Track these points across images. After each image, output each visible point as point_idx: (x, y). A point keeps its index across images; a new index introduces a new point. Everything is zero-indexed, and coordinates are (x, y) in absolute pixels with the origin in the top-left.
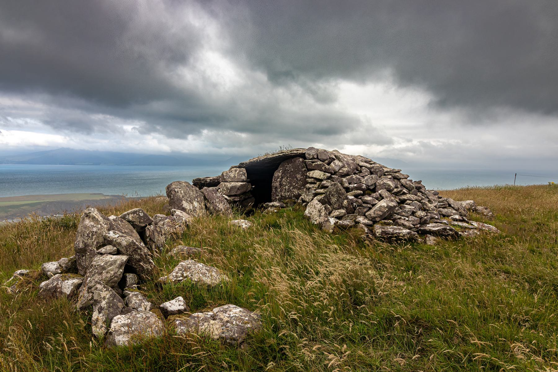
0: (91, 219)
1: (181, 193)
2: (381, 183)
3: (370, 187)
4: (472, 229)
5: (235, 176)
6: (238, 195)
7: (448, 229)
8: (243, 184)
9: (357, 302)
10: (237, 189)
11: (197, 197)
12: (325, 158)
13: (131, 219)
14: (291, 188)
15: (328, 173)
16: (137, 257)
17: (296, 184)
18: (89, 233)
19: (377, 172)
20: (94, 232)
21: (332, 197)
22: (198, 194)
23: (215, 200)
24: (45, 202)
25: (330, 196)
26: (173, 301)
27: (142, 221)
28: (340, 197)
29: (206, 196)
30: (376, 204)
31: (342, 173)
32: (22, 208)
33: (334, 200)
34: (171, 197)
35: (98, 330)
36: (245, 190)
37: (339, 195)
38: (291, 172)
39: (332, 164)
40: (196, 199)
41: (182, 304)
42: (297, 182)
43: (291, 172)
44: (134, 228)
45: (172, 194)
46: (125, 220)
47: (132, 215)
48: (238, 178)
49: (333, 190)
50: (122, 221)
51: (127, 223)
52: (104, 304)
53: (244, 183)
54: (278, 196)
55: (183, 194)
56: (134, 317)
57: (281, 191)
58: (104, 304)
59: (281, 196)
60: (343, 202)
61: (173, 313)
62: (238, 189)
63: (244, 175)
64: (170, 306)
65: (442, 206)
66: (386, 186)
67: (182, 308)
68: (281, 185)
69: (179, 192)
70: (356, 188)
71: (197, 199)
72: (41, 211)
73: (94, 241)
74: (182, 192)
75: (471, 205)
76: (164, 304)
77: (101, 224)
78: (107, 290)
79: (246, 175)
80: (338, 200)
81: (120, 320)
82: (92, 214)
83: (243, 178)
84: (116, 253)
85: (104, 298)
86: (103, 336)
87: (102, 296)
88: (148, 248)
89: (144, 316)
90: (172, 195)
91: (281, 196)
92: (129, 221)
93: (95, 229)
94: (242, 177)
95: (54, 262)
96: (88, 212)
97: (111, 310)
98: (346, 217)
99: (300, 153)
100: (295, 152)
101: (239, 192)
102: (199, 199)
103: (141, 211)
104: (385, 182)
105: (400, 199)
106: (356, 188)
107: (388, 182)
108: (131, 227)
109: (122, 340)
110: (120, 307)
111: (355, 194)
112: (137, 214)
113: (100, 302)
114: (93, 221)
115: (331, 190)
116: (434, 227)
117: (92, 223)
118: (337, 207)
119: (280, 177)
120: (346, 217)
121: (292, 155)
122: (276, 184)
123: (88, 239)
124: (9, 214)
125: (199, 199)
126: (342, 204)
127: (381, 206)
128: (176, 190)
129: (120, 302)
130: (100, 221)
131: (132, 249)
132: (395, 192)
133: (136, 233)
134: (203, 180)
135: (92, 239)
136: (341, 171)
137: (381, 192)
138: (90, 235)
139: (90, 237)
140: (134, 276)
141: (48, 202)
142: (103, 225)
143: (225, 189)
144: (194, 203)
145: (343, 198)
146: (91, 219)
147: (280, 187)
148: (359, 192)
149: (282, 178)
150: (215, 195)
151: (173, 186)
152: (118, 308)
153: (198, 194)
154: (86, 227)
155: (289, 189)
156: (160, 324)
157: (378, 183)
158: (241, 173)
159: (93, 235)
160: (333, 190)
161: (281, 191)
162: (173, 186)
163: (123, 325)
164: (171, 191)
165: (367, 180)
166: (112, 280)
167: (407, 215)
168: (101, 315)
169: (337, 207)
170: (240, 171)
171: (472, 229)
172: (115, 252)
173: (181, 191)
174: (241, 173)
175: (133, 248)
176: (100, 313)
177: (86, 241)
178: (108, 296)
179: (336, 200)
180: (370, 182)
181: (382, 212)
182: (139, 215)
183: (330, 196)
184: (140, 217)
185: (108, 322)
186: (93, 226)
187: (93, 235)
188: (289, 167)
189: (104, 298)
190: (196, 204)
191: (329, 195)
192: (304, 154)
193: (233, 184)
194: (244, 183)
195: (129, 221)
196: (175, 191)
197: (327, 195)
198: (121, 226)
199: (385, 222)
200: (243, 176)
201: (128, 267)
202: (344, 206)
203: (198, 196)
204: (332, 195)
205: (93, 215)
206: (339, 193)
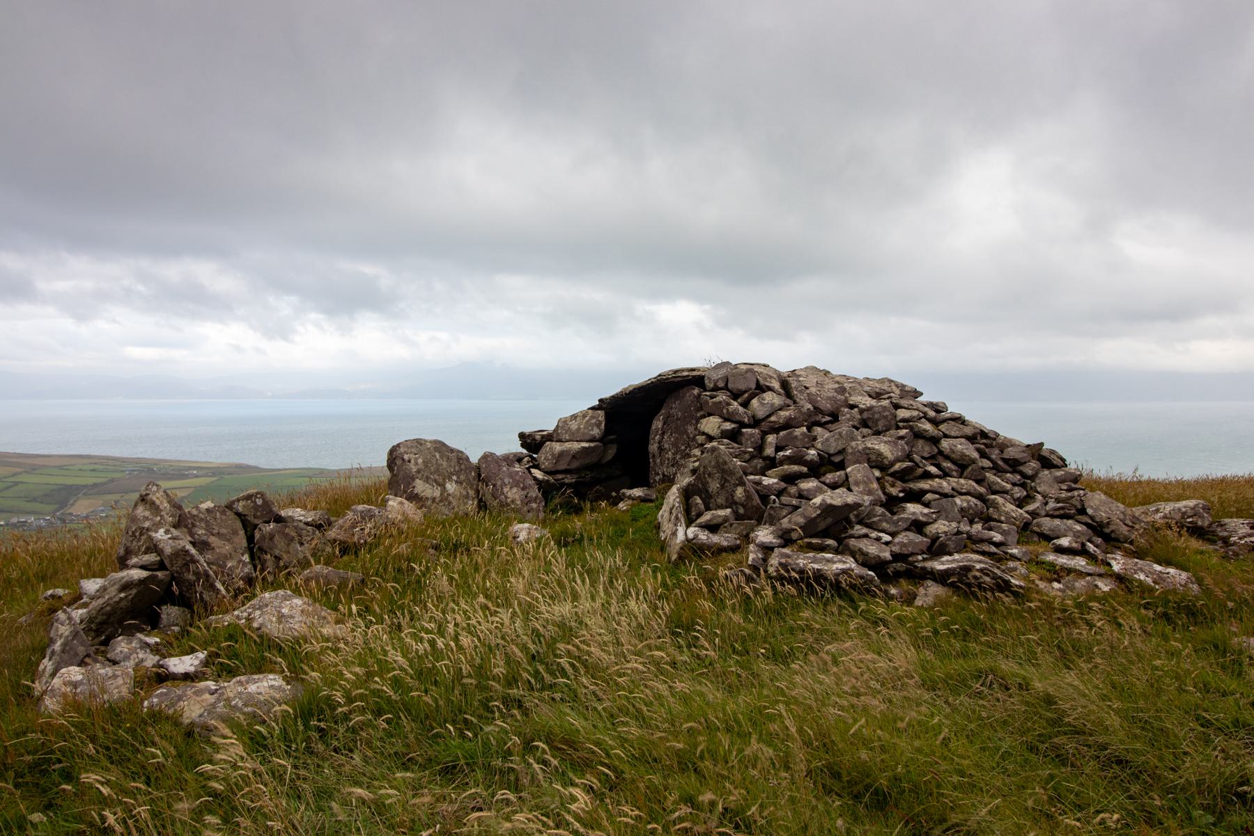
0: (148, 506)
1: (416, 464)
2: (860, 448)
3: (833, 458)
4: (1089, 575)
5: (579, 429)
6: (574, 470)
7: (978, 570)
8: (590, 447)
9: (688, 716)
10: (570, 457)
12: (742, 387)
13: (240, 509)
14: (678, 456)
15: (733, 422)
17: (686, 447)
18: (136, 531)
19: (877, 420)
20: (143, 528)
21: (709, 480)
22: (463, 467)
25: (706, 476)
27: (259, 514)
28: (726, 481)
31: (774, 422)
33: (714, 486)
34: (394, 470)
36: (595, 459)
37: (725, 476)
38: (678, 419)
39: (755, 402)
42: (689, 444)
43: (678, 419)
45: (395, 464)
46: (232, 510)
47: (244, 503)
48: (584, 434)
49: (710, 462)
53: (592, 445)
54: (658, 474)
57: (662, 464)
58: (57, 646)
59: (664, 475)
60: (734, 491)
63: (598, 425)
64: (175, 665)
65: (1057, 513)
66: (871, 456)
68: (661, 449)
69: (413, 461)
70: (791, 460)
71: (458, 477)
73: (143, 545)
74: (420, 461)
75: (1184, 513)
76: (197, 662)
77: (161, 516)
79: (603, 425)
80: (722, 486)
82: (151, 496)
83: (596, 432)
84: (156, 567)
87: (59, 633)
90: (396, 468)
91: (664, 475)
92: (238, 514)
94: (592, 430)
96: (144, 493)
98: (725, 527)
99: (694, 377)
100: (685, 374)
101: (575, 465)
102: (462, 477)
103: (259, 496)
104: (870, 446)
106: (791, 460)
107: (877, 447)
110: (80, 654)
111: (783, 473)
112: (252, 502)
115: (707, 462)
116: (828, 561)
117: (147, 513)
118: (724, 503)
119: (660, 432)
120: (725, 527)
121: (679, 379)
122: (653, 448)
123: (132, 542)
125: (462, 477)
126: (732, 496)
128: (406, 457)
129: (82, 645)
130: (161, 511)
131: (180, 562)
132: (896, 472)
134: (529, 435)
135: (139, 540)
136: (773, 418)
137: (852, 470)
138: (137, 534)
139: (136, 537)
140: (184, 612)
142: (166, 516)
143: (550, 457)
145: (733, 482)
146: (148, 506)
147: (660, 453)
148: (795, 468)
149: (663, 433)
150: (505, 469)
151: (402, 450)
152: (76, 654)
153: (463, 467)
155: (674, 459)
157: (852, 448)
159: (141, 534)
160: (710, 462)
161: (662, 464)
162: (402, 450)
164: (395, 459)
166: (103, 611)
167: (892, 529)
168: (51, 663)
169: (724, 503)
170: (592, 417)
171: (1089, 575)
172: (155, 565)
173: (416, 459)
175: (184, 559)
177: (129, 544)
178: (67, 633)
179: (718, 485)
180: (834, 444)
182: (255, 502)
183: (706, 476)
184: (256, 507)
186: (146, 518)
188: (675, 408)
189: (61, 636)
190: (451, 487)
191: (704, 474)
192: (704, 377)
193: (567, 445)
194: (592, 445)
195: (238, 514)
196: (403, 460)
197: (700, 474)
198: (219, 521)
199: (810, 543)
200: (595, 428)
202: (738, 500)
203: (461, 470)
204: (710, 475)
205: (151, 499)
206: (723, 471)
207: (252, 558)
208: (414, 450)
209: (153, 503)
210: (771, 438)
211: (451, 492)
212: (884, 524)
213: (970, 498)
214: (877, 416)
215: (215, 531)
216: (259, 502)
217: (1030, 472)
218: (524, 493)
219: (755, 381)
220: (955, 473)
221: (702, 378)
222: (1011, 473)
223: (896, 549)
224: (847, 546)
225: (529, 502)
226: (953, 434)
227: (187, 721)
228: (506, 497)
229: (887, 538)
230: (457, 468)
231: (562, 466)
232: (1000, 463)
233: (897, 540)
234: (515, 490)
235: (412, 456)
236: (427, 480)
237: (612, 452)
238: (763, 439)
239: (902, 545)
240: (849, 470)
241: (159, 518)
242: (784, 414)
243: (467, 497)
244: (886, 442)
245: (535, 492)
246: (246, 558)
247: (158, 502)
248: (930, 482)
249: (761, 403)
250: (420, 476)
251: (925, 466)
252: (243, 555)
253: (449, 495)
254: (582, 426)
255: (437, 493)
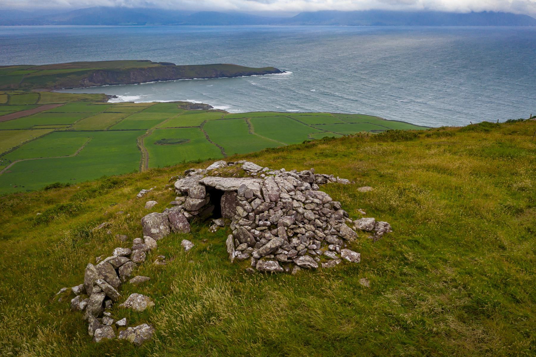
1: (151, 223)
11: (163, 222)
13: (112, 263)
16: (110, 293)
19: (287, 207)
22: (164, 219)
23: (176, 221)
24: (91, 71)
26: (121, 320)
29: (170, 219)
30: (271, 239)
32: (68, 76)
35: (91, 334)
40: (162, 224)
41: (125, 322)
44: (114, 267)
50: (107, 264)
51: (110, 265)
52: (92, 324)
55: (152, 224)
56: (103, 330)
58: (92, 324)
61: (121, 326)
62: (197, 206)
63: (203, 193)
67: (124, 324)
69: (149, 223)
72: (88, 81)
74: (152, 222)
78: (93, 318)
80: (244, 237)
81: (98, 331)
83: (203, 195)
85: (92, 322)
86: (92, 336)
88: (120, 280)
89: (107, 329)
93: (92, 277)
94: (202, 195)
95: (76, 287)
97: (95, 326)
102: (164, 223)
105: (294, 232)
107: (286, 222)
108: (112, 267)
109: (98, 340)
113: (91, 323)
114: (91, 272)
117: (91, 273)
124: (58, 84)
127: (266, 247)
128: (147, 222)
133: (115, 270)
135: (91, 281)
141: (94, 70)
144: (161, 227)
150: (177, 217)
152: (97, 326)
153: (164, 219)
154: (88, 276)
156: (113, 333)
158: (202, 191)
159: (91, 280)
163: (99, 334)
165: (273, 218)
174: (202, 191)
176: (91, 327)
178: (93, 321)
180: (275, 219)
181: (266, 251)
184: (116, 262)
185: (94, 331)
187: (91, 280)
189: (92, 322)
190: (162, 227)
196: (147, 223)
200: (203, 194)
201: (107, 298)
207: (119, 277)
208: (149, 219)
209: (91, 270)
210: (257, 217)
211: (161, 229)
212: (286, 248)
213: (310, 232)
214: (287, 206)
215: (107, 271)
216: (117, 260)
217: (329, 216)
218: (183, 224)
219: (253, 194)
220: (307, 223)
221: (236, 191)
222: (324, 217)
223: (289, 256)
224: (276, 258)
225: (185, 226)
226: (308, 209)
227: (132, 342)
228: (178, 227)
229: (286, 253)
230: (162, 220)
231: (194, 209)
232: (321, 214)
233: (289, 253)
234: (181, 223)
235: (149, 221)
236: (154, 228)
237: (208, 200)
238: (255, 217)
239: (291, 255)
240: (278, 228)
241: (94, 274)
242: (261, 207)
243: (166, 229)
244: (289, 219)
245: (186, 223)
246: (117, 278)
247: (93, 269)
248: (300, 230)
249: (255, 203)
250: (152, 227)
251: (299, 224)
252: (116, 277)
253: (161, 230)
254: (198, 193)
255: (158, 231)
